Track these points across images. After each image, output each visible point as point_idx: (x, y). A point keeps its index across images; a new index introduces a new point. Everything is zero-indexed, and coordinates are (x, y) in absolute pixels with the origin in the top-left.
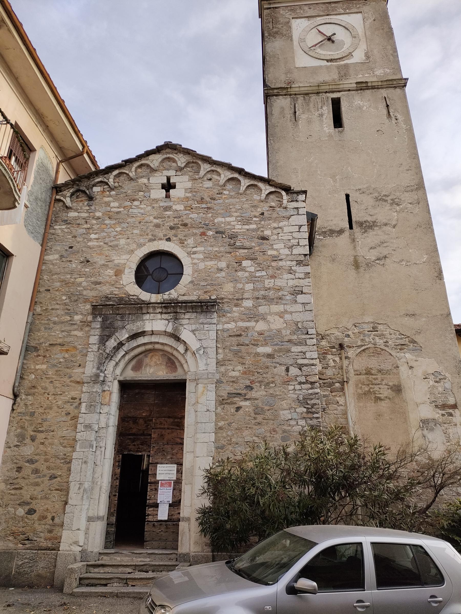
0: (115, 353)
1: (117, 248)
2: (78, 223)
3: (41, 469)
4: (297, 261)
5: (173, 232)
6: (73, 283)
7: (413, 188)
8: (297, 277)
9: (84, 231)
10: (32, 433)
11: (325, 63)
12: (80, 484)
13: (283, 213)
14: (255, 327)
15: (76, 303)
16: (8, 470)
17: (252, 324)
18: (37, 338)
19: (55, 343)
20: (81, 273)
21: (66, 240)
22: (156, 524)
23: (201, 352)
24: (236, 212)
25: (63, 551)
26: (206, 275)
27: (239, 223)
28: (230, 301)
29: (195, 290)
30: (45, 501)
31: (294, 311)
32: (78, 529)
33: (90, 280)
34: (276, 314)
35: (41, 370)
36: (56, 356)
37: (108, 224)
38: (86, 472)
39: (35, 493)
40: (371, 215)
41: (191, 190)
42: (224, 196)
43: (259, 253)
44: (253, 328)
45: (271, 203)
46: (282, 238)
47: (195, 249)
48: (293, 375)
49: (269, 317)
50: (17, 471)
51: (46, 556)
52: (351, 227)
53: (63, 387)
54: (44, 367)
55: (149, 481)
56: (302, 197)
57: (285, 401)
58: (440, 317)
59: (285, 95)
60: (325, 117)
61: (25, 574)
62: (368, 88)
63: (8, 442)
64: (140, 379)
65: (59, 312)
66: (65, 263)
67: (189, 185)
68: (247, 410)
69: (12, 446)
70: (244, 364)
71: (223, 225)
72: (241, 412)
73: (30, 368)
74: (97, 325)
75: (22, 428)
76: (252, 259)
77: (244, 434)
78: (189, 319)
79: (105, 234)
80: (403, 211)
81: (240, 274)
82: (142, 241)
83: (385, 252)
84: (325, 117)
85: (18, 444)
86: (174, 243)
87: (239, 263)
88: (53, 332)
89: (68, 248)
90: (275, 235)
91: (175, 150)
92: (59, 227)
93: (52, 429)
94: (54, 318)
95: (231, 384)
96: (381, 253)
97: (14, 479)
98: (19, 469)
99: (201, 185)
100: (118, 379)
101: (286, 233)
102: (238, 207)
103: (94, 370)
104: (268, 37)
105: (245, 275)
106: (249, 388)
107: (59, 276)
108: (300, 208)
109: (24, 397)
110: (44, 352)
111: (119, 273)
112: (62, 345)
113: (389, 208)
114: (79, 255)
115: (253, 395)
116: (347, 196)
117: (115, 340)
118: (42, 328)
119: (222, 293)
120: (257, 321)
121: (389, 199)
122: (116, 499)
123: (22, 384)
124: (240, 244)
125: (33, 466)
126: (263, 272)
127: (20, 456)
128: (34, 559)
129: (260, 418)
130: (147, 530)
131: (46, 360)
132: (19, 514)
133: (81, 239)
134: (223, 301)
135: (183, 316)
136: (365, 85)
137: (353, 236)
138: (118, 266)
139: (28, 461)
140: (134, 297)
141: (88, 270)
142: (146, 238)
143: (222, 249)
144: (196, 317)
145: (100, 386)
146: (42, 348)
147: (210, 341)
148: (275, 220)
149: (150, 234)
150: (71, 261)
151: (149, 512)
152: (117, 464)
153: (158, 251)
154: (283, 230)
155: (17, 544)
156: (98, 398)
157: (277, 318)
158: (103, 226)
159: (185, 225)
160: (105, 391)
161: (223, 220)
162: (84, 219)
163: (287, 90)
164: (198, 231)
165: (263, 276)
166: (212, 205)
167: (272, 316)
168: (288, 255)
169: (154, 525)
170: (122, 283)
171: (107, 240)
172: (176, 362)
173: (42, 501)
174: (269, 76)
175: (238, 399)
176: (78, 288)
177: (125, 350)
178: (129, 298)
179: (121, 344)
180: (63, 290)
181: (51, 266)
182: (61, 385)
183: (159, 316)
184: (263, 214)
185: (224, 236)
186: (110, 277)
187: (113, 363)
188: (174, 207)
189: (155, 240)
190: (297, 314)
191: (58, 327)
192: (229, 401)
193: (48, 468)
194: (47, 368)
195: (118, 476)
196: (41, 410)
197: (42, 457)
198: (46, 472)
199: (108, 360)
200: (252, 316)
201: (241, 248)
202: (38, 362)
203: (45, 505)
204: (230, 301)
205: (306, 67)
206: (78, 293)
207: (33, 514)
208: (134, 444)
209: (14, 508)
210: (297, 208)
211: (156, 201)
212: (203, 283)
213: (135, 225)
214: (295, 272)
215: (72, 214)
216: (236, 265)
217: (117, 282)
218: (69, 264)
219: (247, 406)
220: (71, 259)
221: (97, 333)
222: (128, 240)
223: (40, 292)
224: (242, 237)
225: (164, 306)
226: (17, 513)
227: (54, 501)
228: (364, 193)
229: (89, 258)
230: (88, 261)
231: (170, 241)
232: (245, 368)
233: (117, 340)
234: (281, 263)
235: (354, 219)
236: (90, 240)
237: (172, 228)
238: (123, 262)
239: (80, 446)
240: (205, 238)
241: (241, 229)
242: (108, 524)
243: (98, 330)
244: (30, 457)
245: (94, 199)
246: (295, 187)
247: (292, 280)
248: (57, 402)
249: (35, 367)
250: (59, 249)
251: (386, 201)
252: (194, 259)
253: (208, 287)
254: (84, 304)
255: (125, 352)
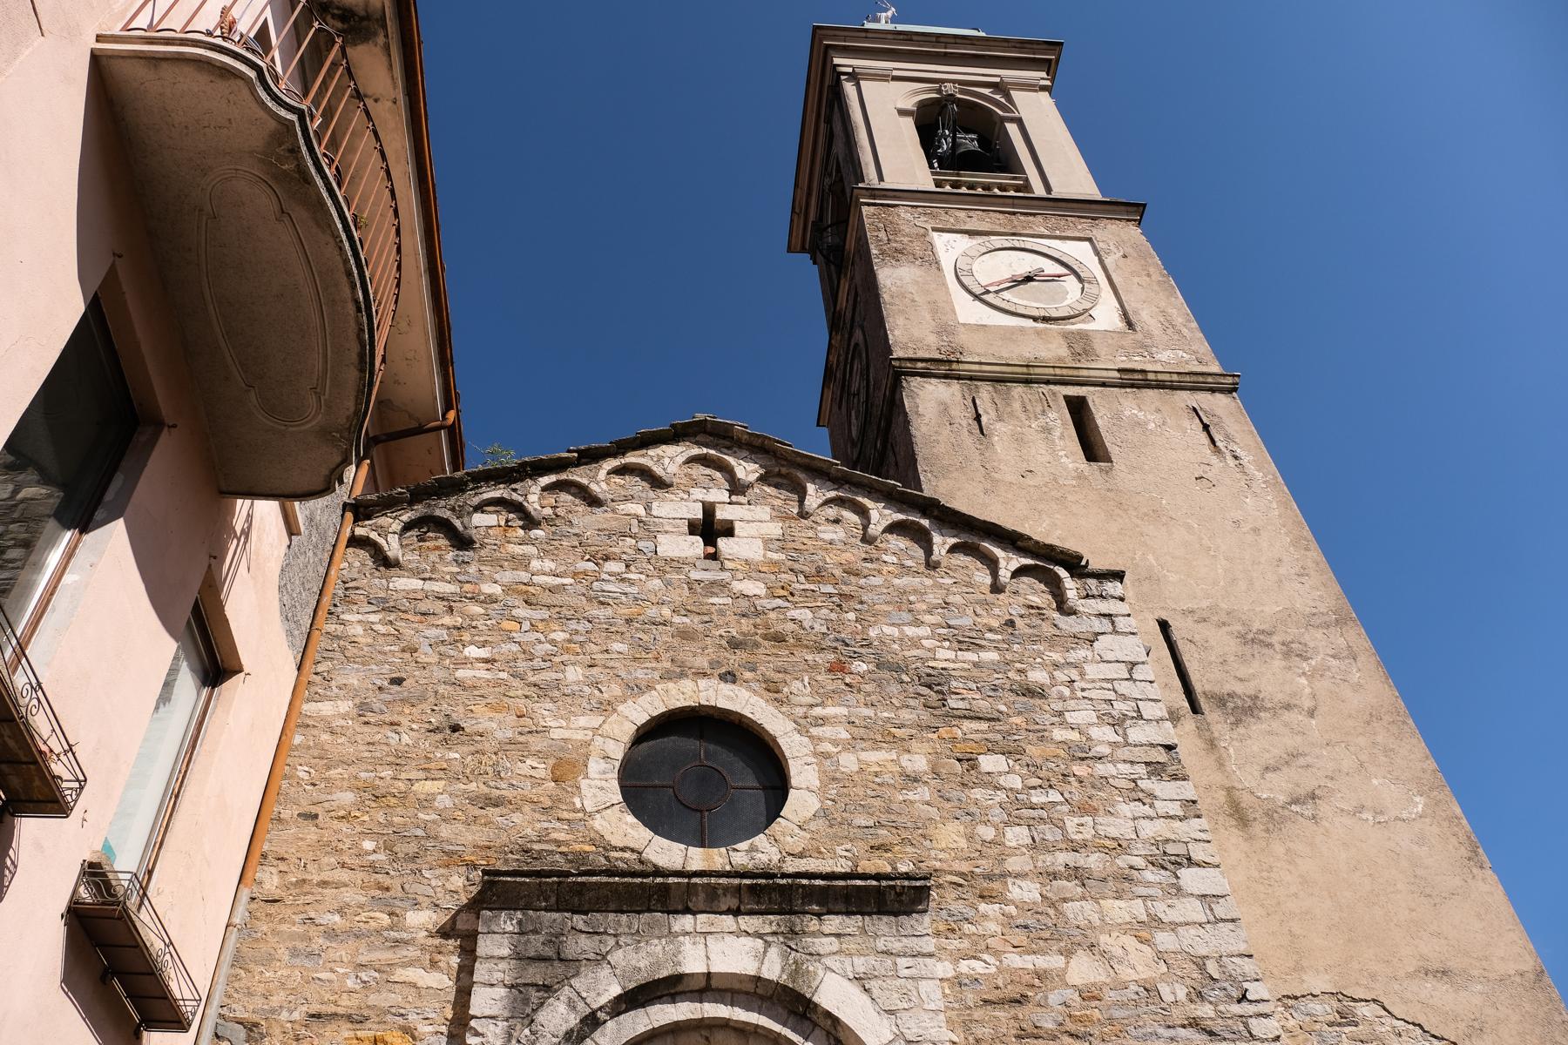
1: (556, 693)
5: (741, 656)
6: (403, 797)
7: (1327, 618)
9: (444, 635)
11: (1030, 323)
14: (1065, 970)
17: (1053, 962)
18: (261, 989)
19: (331, 1009)
20: (432, 766)
21: (380, 657)
24: (930, 613)
27: (947, 644)
28: (961, 881)
29: (837, 839)
37: (525, 619)
40: (1241, 680)
41: (782, 543)
42: (885, 569)
43: (1023, 732)
44: (1062, 974)
46: (1084, 694)
52: (1195, 709)
56: (1112, 587)
58: (1518, 979)
59: (946, 377)
60: (1057, 433)
62: (1148, 385)
65: (350, 896)
66: (376, 729)
67: (775, 529)
74: (501, 945)
78: (838, 936)
79: (515, 648)
80: (1321, 676)
82: (640, 674)
83: (1308, 783)
84: (1058, 434)
86: (749, 689)
87: (970, 761)
88: (325, 969)
91: (724, 438)
94: (329, 916)
96: (1298, 785)
101: (1093, 681)
104: (881, 256)
107: (352, 770)
108: (1116, 616)
111: (566, 769)
113: (1284, 663)
114: (427, 707)
116: (1164, 626)
117: (571, 1006)
120: (1068, 953)
121: (1275, 639)
133: (434, 659)
136: (1140, 377)
137: (1207, 734)
141: (457, 756)
142: (653, 669)
143: (907, 717)
146: (277, 1031)
147: (925, 1016)
149: (665, 656)
153: (692, 709)
159: (779, 639)
161: (895, 631)
162: (443, 599)
163: (950, 366)
168: (1114, 744)
170: (578, 805)
174: (896, 332)
176: (421, 815)
178: (607, 858)
180: (366, 818)
181: (325, 737)
183: (728, 921)
185: (905, 678)
186: (537, 782)
188: (738, 586)
189: (682, 675)
191: (342, 951)
200: (1046, 934)
205: (985, 326)
206: (420, 832)
212: (861, 820)
214: (1152, 796)
215: (404, 583)
218: (390, 734)
220: (396, 718)
221: (500, 976)
222: (594, 671)
223: (279, 820)
225: (750, 887)
228: (1205, 621)
229: (458, 716)
230: (455, 728)
233: (581, 1005)
234: (1101, 769)
235: (1198, 687)
236: (466, 662)
238: (579, 736)
240: (848, 680)
243: (503, 965)
246: (1096, 563)
250: (356, 682)
251: (1269, 645)
254: (442, 871)
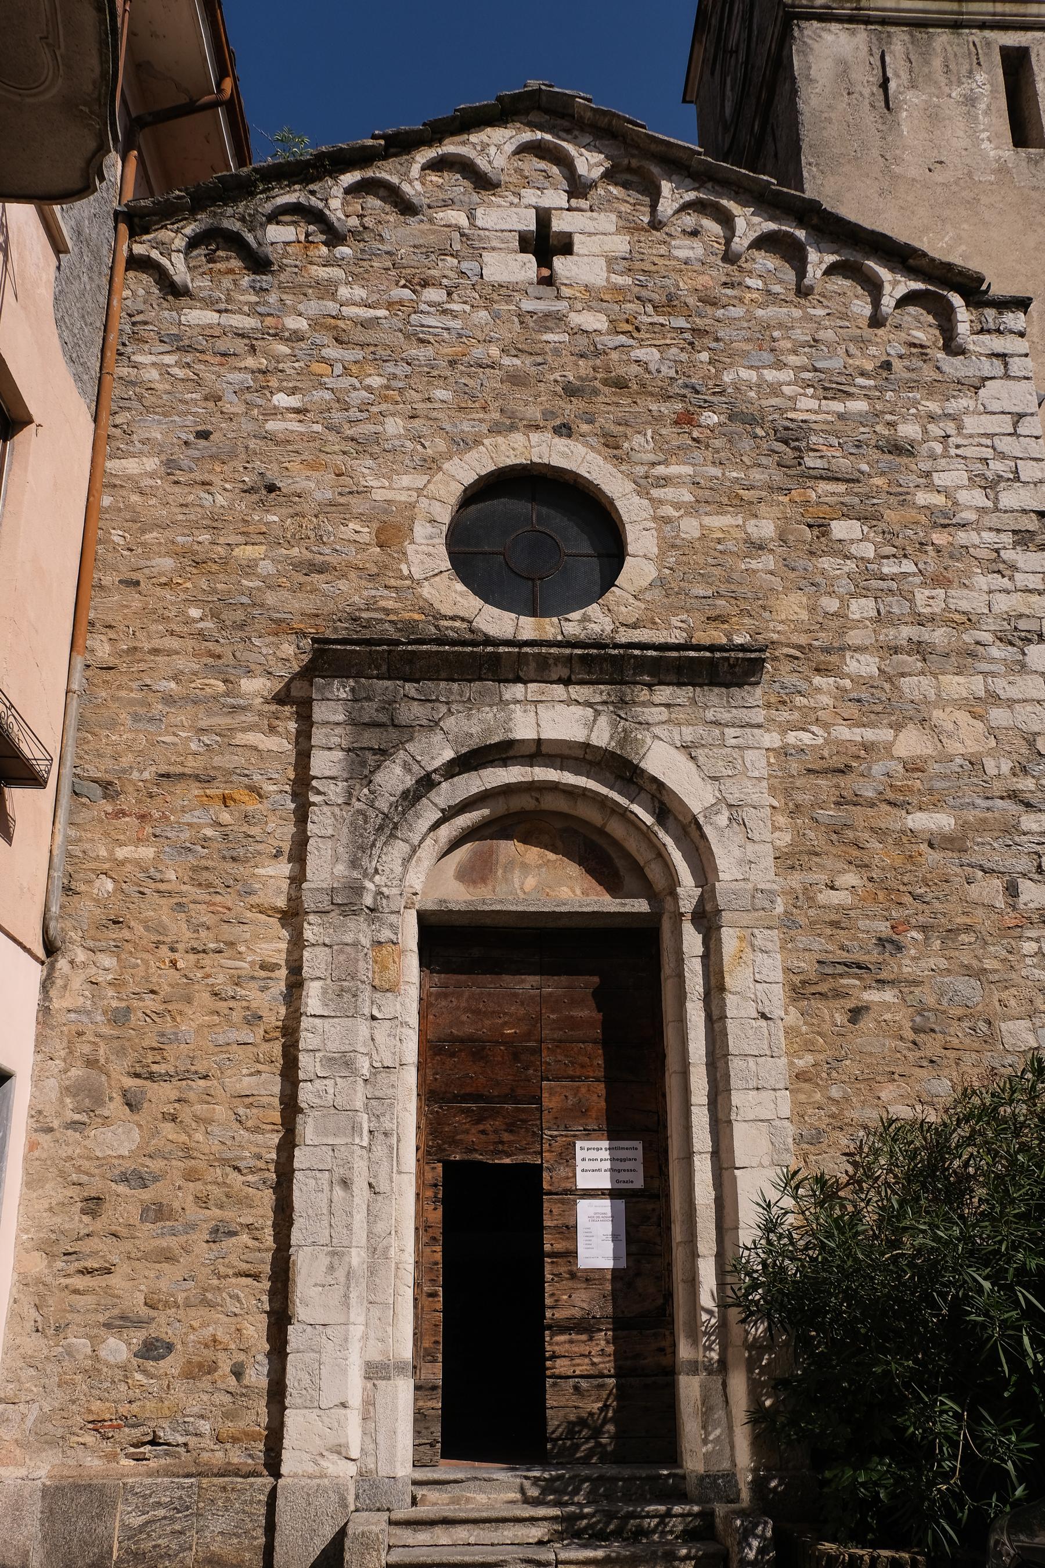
0: (404, 813)
2: (223, 349)
3: (176, 1205)
4: (1015, 532)
5: (578, 405)
6: (224, 562)
8: (1020, 585)
10: (129, 1082)
12: (334, 1254)
13: (953, 366)
14: (892, 744)
15: (240, 634)
16: (50, 1209)
17: (884, 734)
20: (251, 529)
21: (182, 407)
22: (584, 1384)
23: (722, 819)
24: (795, 352)
25: (295, 1475)
26: (710, 560)
28: (798, 654)
29: (674, 610)
30: (203, 1311)
31: (1020, 696)
32: (344, 1405)
33: (287, 557)
34: (961, 704)
35: (137, 863)
36: (187, 818)
37: (336, 360)
38: (349, 1214)
39: (164, 1285)
41: (628, 263)
43: (884, 495)
44: (889, 747)
45: (914, 333)
46: (959, 452)
47: (661, 470)
48: (1031, 905)
49: (937, 714)
50: (83, 1212)
51: (233, 1496)
53: (226, 926)
54: (147, 852)
55: (547, 1247)
56: (1014, 320)
57: (1013, 991)
61: (161, 1557)
63: (40, 1112)
64: (498, 907)
65: (181, 663)
66: (187, 489)
67: (620, 244)
68: (888, 1016)
69: (56, 1124)
70: (867, 866)
71: (752, 394)
72: (867, 1023)
73: (93, 855)
74: (335, 712)
75: (91, 1063)
76: (862, 518)
77: (883, 1095)
78: (668, 706)
81: (826, 563)
82: (466, 427)
85: (77, 1117)
87: (821, 528)
88: (168, 733)
89: (191, 437)
90: (935, 439)
91: (563, 116)
92: (153, 358)
93: (200, 1067)
94: (165, 683)
95: (828, 931)
97: (78, 1239)
98: (93, 1205)
99: (662, 252)
100: (417, 907)
102: (800, 334)
103: (341, 869)
105: (846, 569)
106: (890, 944)
108: (1012, 356)
109: (81, 956)
110: (139, 801)
112: (204, 779)
115: (906, 970)
117: (407, 768)
118: (124, 717)
119: (771, 625)
120: (898, 727)
122: (440, 1306)
123: (69, 910)
124: (819, 463)
125: (146, 1195)
126: (905, 561)
127: (89, 1158)
128: (187, 1508)
129: (932, 1046)
130: (555, 1404)
131: (149, 830)
132: (112, 1360)
133: (240, 409)
134: (777, 654)
135: (644, 694)
138: (386, 511)
139: (124, 1178)
140: (457, 624)
141: (276, 518)
143: (758, 477)
144: (694, 701)
145: (364, 926)
146: (131, 789)
148: (932, 389)
149: (494, 406)
150: (209, 484)
151: (556, 1348)
152: (429, 1193)
153: (522, 467)
154: (960, 428)
155: (112, 1457)
156: (362, 964)
157: (963, 717)
158: (318, 368)
159: (620, 384)
160: (380, 943)
161: (751, 375)
162: (243, 336)
164: (670, 409)
165: (905, 575)
166: (708, 321)
167: (948, 710)
168: (982, 510)
169: (576, 1388)
170: (406, 572)
171: (337, 416)
172: (614, 855)
173: (192, 1312)
175: (857, 982)
176: (244, 582)
177: (443, 806)
178: (437, 627)
179: (426, 783)
180: (189, 585)
181: (135, 498)
182: (217, 918)
184: (887, 366)
185: (760, 432)
186: (362, 547)
187: (399, 849)
188: (576, 319)
189: (512, 428)
190: (1029, 708)
191: (181, 717)
192: (823, 988)
193: (202, 1201)
194: (157, 857)
195: (438, 1233)
196: (150, 1003)
197: (174, 1162)
198: (194, 1213)
199: (383, 838)
200: (879, 708)
201: (822, 478)
202: (122, 837)
203: (203, 1326)
204: (798, 654)
206: (245, 600)
207: (163, 1357)
208: (481, 1127)
209: (87, 1336)
210: (1002, 356)
211: (506, 290)
213: (435, 373)
214: (1014, 568)
215: (198, 316)
216: (808, 535)
217: (386, 567)
219: (887, 1006)
220: (206, 477)
221: (337, 740)
222: (416, 423)
223: (101, 587)
224: (821, 441)
225: (581, 657)
226: (103, 1354)
227: (237, 1311)
229: (273, 474)
230: (271, 488)
231: (569, 436)
232: (871, 879)
233: (416, 768)
234: (963, 537)
236: (275, 412)
237: (571, 391)
238: (403, 497)
239: (316, 1127)
240: (695, 434)
241: (816, 412)
242: (417, 1388)
244: (129, 1165)
245: (276, 268)
247: (1003, 595)
248: (208, 976)
249: (111, 852)
250: (159, 436)
252: (661, 502)
253: (721, 602)
254: (271, 639)
255: (443, 811)
